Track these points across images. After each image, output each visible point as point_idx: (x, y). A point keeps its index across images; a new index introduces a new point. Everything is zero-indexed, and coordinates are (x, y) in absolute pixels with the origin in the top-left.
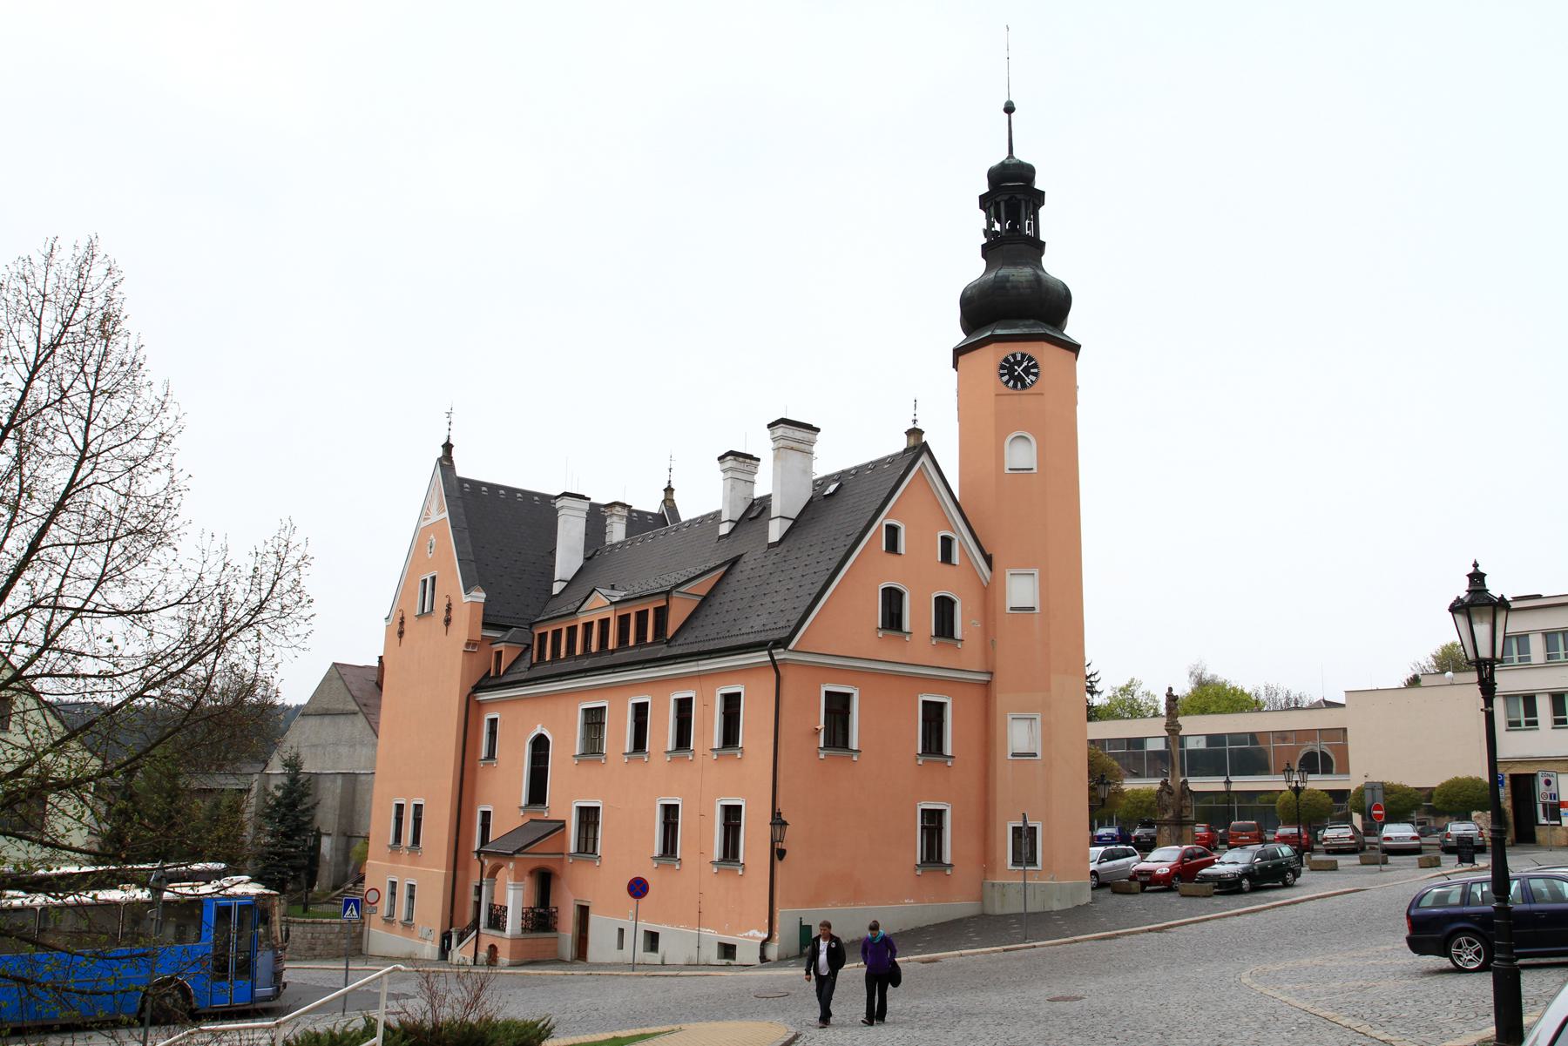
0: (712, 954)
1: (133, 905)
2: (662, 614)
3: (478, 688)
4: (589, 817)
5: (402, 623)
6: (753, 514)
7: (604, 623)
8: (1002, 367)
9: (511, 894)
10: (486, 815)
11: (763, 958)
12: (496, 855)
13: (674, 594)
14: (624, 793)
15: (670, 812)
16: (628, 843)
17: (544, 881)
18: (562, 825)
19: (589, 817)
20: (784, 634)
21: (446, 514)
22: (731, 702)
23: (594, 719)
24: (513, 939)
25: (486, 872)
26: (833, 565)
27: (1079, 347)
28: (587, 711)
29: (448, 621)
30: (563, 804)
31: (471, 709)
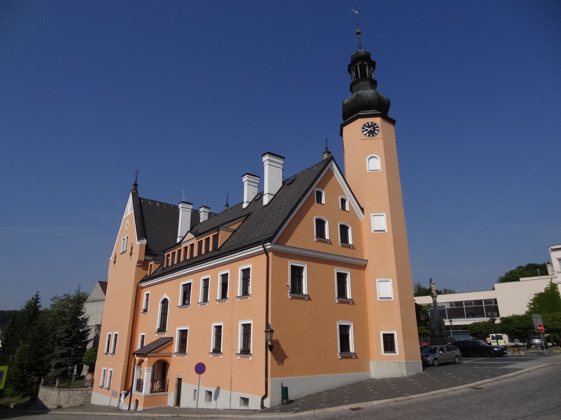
1: (77, 368)
2: (216, 238)
3: (143, 281)
4: (184, 333)
5: (115, 258)
6: (258, 197)
7: (192, 245)
8: (376, 134)
10: (143, 336)
11: (262, 406)
12: (143, 353)
13: (221, 228)
14: (195, 322)
15: (219, 329)
16: (200, 346)
17: (161, 370)
18: (171, 339)
19: (184, 333)
20: (271, 235)
21: (133, 211)
23: (187, 288)
24: (146, 397)
25: (137, 363)
27: (248, 399)
28: (183, 285)
29: (131, 254)
31: (138, 290)
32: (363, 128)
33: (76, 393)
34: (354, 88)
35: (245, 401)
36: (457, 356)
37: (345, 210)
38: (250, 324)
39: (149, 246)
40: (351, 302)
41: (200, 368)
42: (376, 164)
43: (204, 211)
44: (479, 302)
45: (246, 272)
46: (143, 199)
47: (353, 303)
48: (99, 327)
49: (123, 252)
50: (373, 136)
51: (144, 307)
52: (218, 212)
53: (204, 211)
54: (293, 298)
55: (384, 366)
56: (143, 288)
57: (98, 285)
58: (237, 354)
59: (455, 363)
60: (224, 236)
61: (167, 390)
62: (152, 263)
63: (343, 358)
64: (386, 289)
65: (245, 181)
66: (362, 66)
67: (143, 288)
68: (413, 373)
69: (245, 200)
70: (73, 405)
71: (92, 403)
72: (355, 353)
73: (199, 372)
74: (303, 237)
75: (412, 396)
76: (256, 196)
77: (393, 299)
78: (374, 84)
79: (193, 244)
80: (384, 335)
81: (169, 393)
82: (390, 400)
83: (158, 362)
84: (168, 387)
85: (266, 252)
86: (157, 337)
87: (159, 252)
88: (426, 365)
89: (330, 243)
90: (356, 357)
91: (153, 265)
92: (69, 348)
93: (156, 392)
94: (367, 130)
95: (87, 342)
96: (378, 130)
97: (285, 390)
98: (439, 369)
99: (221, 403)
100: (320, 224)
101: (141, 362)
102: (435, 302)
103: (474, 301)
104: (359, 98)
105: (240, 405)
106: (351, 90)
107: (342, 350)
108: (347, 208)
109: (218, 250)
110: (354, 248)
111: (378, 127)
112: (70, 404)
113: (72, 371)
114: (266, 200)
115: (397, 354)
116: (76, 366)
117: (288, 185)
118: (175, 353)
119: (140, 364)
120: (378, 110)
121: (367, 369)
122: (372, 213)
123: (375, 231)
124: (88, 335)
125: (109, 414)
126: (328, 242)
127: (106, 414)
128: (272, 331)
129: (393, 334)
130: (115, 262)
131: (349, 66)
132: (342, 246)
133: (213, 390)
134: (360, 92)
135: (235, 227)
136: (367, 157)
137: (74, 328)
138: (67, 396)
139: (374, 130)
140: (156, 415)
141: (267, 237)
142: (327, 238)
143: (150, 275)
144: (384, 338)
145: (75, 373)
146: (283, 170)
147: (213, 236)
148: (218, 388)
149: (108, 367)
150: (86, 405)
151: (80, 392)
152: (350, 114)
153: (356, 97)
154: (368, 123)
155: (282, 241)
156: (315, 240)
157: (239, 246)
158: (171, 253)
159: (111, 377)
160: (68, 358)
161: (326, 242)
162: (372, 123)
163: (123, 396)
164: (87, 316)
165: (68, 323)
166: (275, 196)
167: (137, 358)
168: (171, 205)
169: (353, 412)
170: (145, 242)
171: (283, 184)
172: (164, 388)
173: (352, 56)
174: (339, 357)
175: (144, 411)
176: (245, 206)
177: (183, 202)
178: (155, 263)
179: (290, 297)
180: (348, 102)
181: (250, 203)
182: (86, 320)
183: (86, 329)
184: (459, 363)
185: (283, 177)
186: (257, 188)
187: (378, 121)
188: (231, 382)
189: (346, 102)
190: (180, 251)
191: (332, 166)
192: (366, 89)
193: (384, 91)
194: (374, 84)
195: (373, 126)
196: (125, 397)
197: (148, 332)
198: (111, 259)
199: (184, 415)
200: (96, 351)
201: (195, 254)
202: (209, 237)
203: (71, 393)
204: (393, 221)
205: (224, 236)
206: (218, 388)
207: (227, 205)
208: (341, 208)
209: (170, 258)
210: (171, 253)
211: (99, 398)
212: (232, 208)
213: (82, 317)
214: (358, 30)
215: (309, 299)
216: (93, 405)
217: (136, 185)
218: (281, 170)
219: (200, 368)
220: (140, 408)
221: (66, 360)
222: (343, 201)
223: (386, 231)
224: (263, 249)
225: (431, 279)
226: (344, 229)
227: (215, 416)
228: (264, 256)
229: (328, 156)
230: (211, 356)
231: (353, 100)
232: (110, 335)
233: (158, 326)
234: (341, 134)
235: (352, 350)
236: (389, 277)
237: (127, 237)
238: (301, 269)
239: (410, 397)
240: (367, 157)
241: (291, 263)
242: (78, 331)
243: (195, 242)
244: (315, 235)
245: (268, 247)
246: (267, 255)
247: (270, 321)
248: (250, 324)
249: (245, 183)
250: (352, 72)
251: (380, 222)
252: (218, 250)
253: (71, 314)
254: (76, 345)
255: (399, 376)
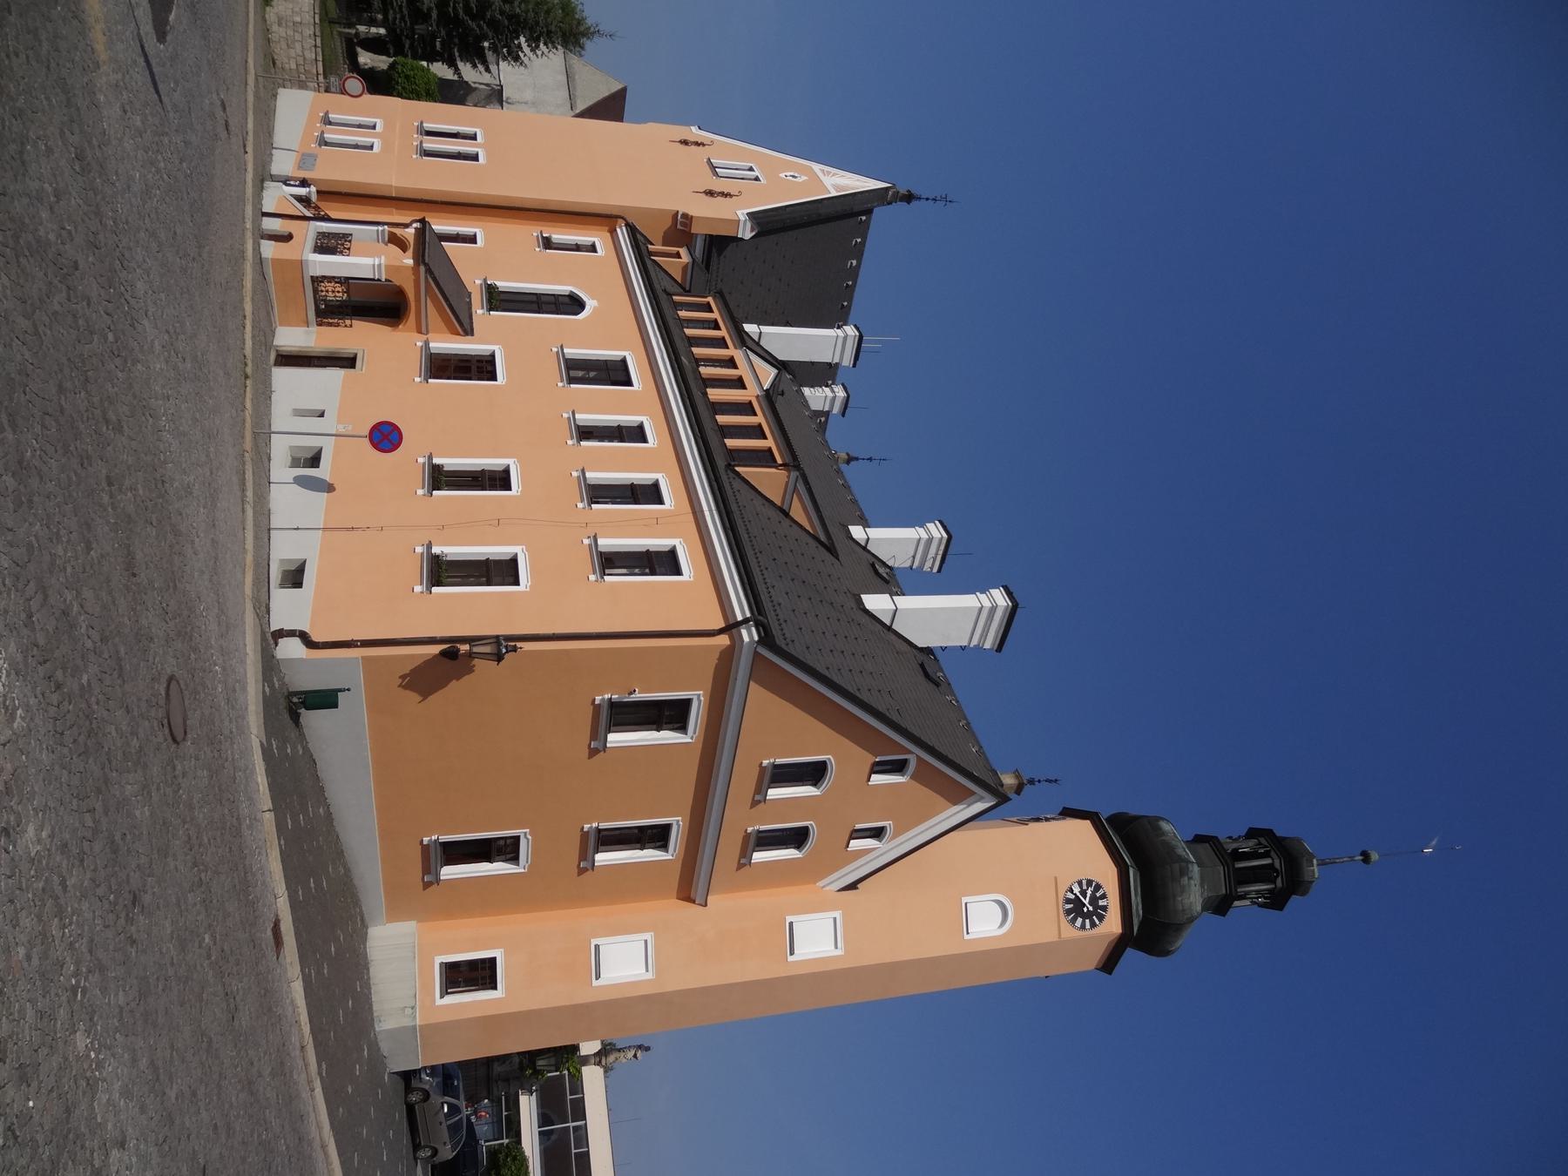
0: (284, 550)
2: (764, 458)
3: (633, 231)
4: (483, 368)
5: (697, 144)
6: (882, 570)
7: (739, 383)
8: (1073, 921)
9: (368, 261)
10: (472, 239)
11: (280, 634)
12: (426, 247)
13: (794, 474)
14: (521, 414)
15: (501, 480)
16: (449, 423)
17: (380, 304)
18: (467, 330)
19: (483, 368)
20: (780, 642)
21: (834, 194)
22: (666, 562)
23: (615, 373)
24: (301, 264)
25: (398, 231)
26: (864, 696)
28: (624, 361)
29: (710, 193)
30: (491, 334)
31: (605, 219)
32: (1089, 882)
33: (307, 46)
34: (1205, 849)
35: (295, 577)
36: (435, 1152)
37: (851, 838)
38: (517, 583)
39: (733, 245)
40: (585, 862)
41: (385, 437)
42: (985, 921)
43: (834, 398)
44: (579, 1111)
45: (666, 562)
46: (868, 222)
47: (581, 871)
48: (496, 96)
49: (713, 168)
50: (1068, 912)
51: (557, 237)
52: (830, 434)
53: (834, 398)
54: (597, 708)
55: (403, 964)
56: (613, 232)
57: (616, 87)
58: (429, 546)
59: (416, 1147)
60: (770, 481)
61: (320, 324)
62: (685, 258)
63: (425, 849)
64: (625, 961)
65: (928, 531)
66: (1268, 869)
67: (613, 232)
68: (385, 1047)
69: (876, 533)
70: (274, 37)
71: (281, 91)
72: (438, 881)
73: (376, 434)
74: (774, 726)
75: (319, 1091)
76: (884, 563)
77: (595, 983)
78: (1220, 906)
79: (744, 387)
80: (493, 960)
81: (314, 329)
82: (306, 1029)
83: (400, 292)
84: (330, 325)
85: (731, 627)
86: (474, 284)
87: (713, 277)
88: (408, 1077)
89: (755, 803)
90: (427, 885)
91: (678, 262)
92: (434, 15)
93: (315, 291)
94: (1084, 893)
95: (452, 63)
96: (1083, 927)
97: (326, 699)
98: (400, 1115)
99: (288, 501)
100: (813, 773)
101: (401, 244)
102: (585, 1060)
103: (588, 1153)
104: (1176, 866)
105: (282, 561)
106: (1199, 839)
107: (446, 846)
108: (856, 844)
109: (730, 467)
110: (740, 866)
111: (1093, 925)
112: (275, 28)
113: (372, 22)
114: (877, 603)
115: (439, 1002)
116: (382, 31)
117: (922, 666)
118: (427, 343)
119: (394, 240)
120: (1142, 924)
121: (395, 914)
122: (844, 915)
123: (791, 924)
124: (475, 66)
125: (250, 157)
126: (758, 797)
127: (250, 149)
128: (499, 658)
129: (495, 988)
130: (685, 142)
131: (1268, 833)
132: (747, 836)
133: (323, 472)
134: (1196, 869)
135: (797, 512)
136: (1005, 894)
137: (493, 24)
138: (298, 19)
139: (1085, 916)
140: (248, 307)
141: (776, 631)
142: (771, 792)
143: (651, 254)
144: (483, 961)
145: (362, 28)
146: (963, 648)
147: (770, 449)
148: (330, 488)
149: (384, 138)
150: (274, 75)
151: (310, 55)
152: (1128, 837)
153: (1181, 859)
154: (1104, 896)
155: (761, 672)
156: (765, 762)
157: (744, 536)
158: (716, 315)
159: (356, 146)
160: (405, 12)
161: (760, 790)
162: (1105, 908)
163: (302, 191)
164: (525, 60)
165: (507, 7)
166: (889, 628)
167: (411, 231)
168: (850, 301)
169: (269, 933)
170: (746, 233)
171: (922, 650)
172: (329, 313)
173: (1299, 841)
174: (426, 840)
175: (260, 261)
176: (857, 532)
177: (861, 337)
178: (685, 268)
179: (598, 699)
180: (1163, 833)
181: (865, 548)
182: (517, 59)
183: (490, 56)
184: (416, 1159)
185: (943, 649)
186: (908, 564)
187: (1112, 925)
188: (347, 529)
189: (1166, 827)
190: (721, 343)
191: (981, 799)
192: (1202, 885)
193: (1201, 937)
194: (1220, 906)
195: (1095, 913)
196: (300, 199)
197: (490, 256)
198: (694, 129)
199: (249, 395)
200: (429, 96)
201: (715, 394)
202: (755, 414)
203: (309, 31)
204: (821, 977)
205: (770, 481)
206: (330, 488)
207: (850, 460)
208: (858, 826)
209: (703, 316)
210: (716, 315)
211: (295, 111)
212: (839, 472)
213: (524, 45)
214: (1374, 856)
215: (593, 752)
216: (275, 96)
217: (909, 198)
218: (965, 643)
219: (385, 437)
220: (269, 249)
221: (401, 7)
222: (877, 833)
223: (790, 959)
224: (740, 618)
225: (648, 1049)
226: (797, 838)
227: (250, 493)
228: (721, 624)
229: (1011, 787)
230: (421, 460)
231: (1170, 849)
232: (474, 137)
233: (503, 285)
234: (1068, 813)
235: (449, 872)
236: (659, 971)
237: (757, 179)
238: (682, 726)
239: (318, 1085)
240: (1005, 894)
241: (699, 699)
242: (486, 38)
243: (751, 393)
244: (779, 761)
245: (744, 632)
246: (721, 631)
247: (527, 646)
248: (517, 583)
249: (921, 530)
250: (1252, 843)
251: (817, 938)
252: (730, 467)
253: (531, 14)
254: (443, 33)
255: (375, 1008)
